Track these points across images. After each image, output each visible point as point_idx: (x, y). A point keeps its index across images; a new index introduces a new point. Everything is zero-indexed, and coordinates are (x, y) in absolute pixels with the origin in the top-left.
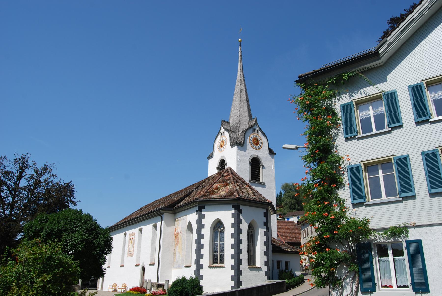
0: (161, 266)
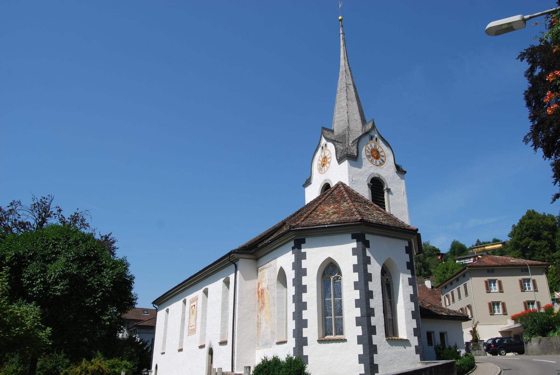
0: (238, 345)
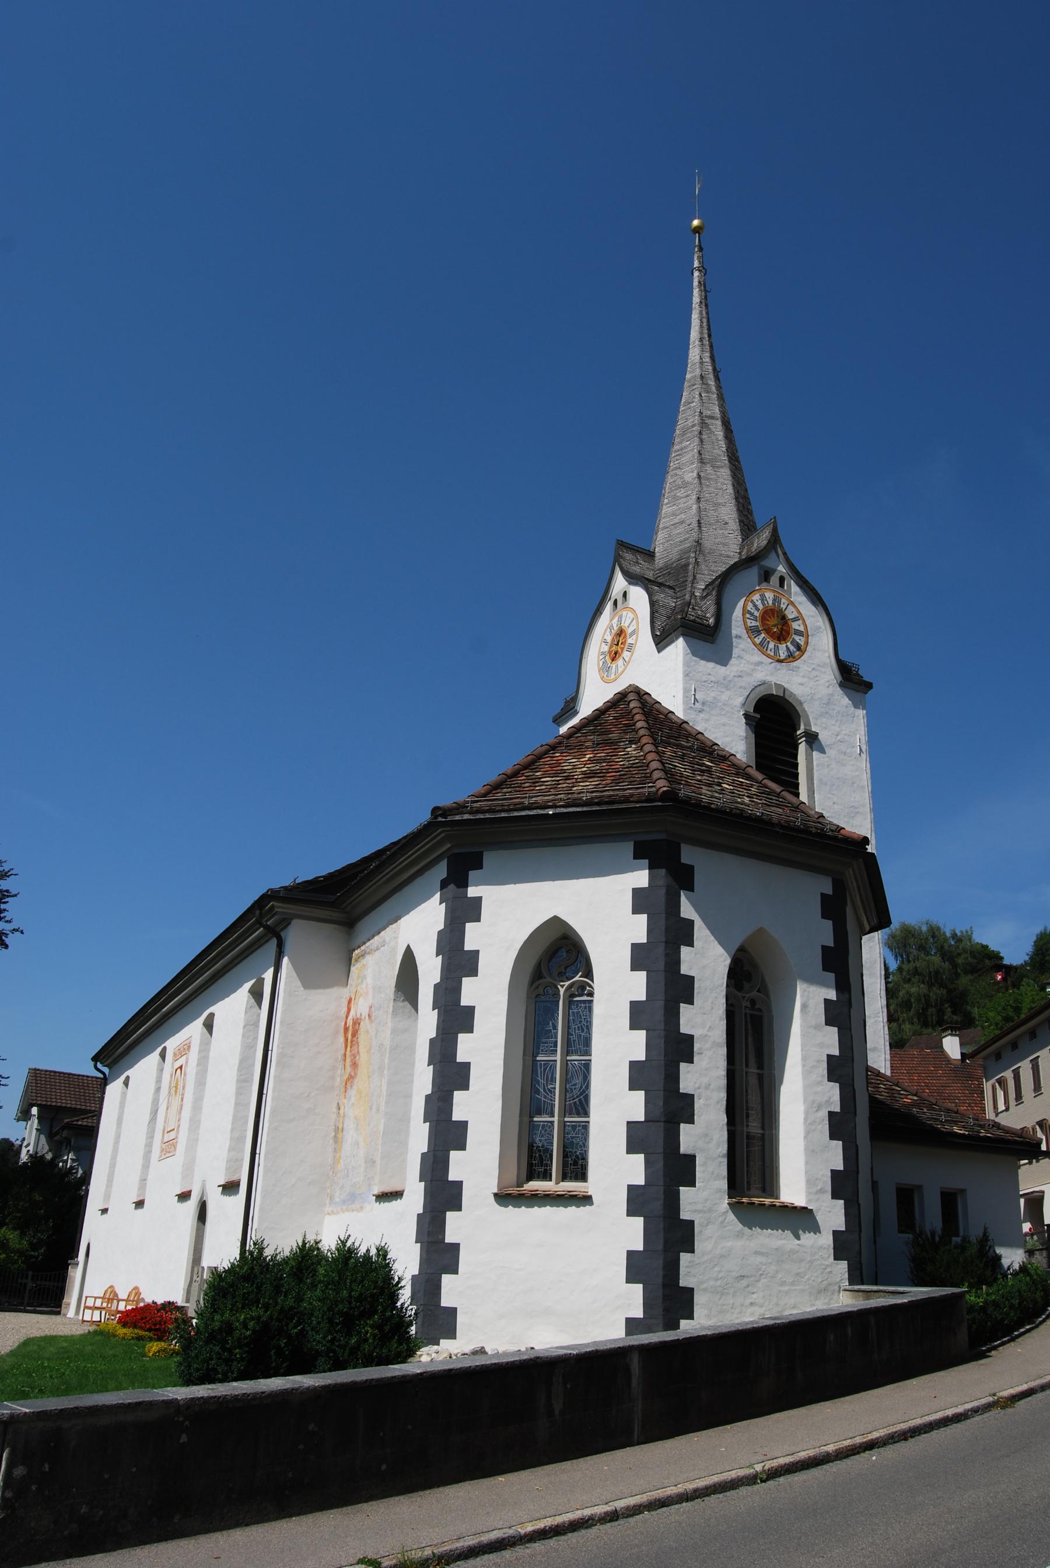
0: (263, 1197)
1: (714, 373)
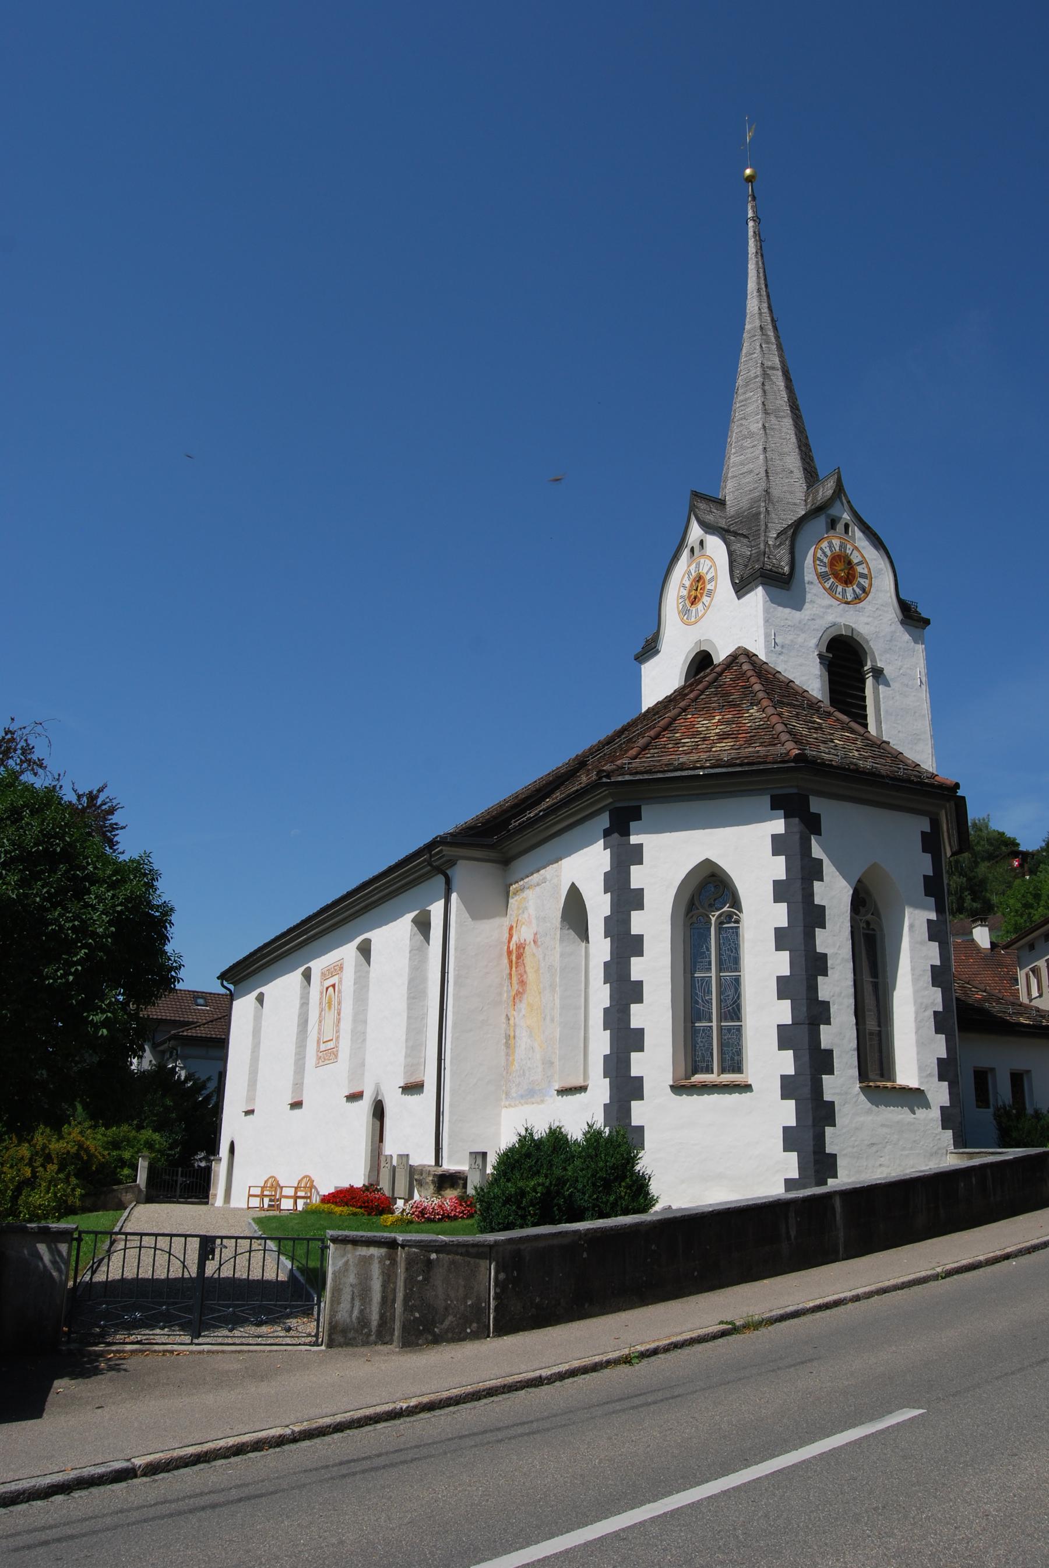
1: (773, 323)
